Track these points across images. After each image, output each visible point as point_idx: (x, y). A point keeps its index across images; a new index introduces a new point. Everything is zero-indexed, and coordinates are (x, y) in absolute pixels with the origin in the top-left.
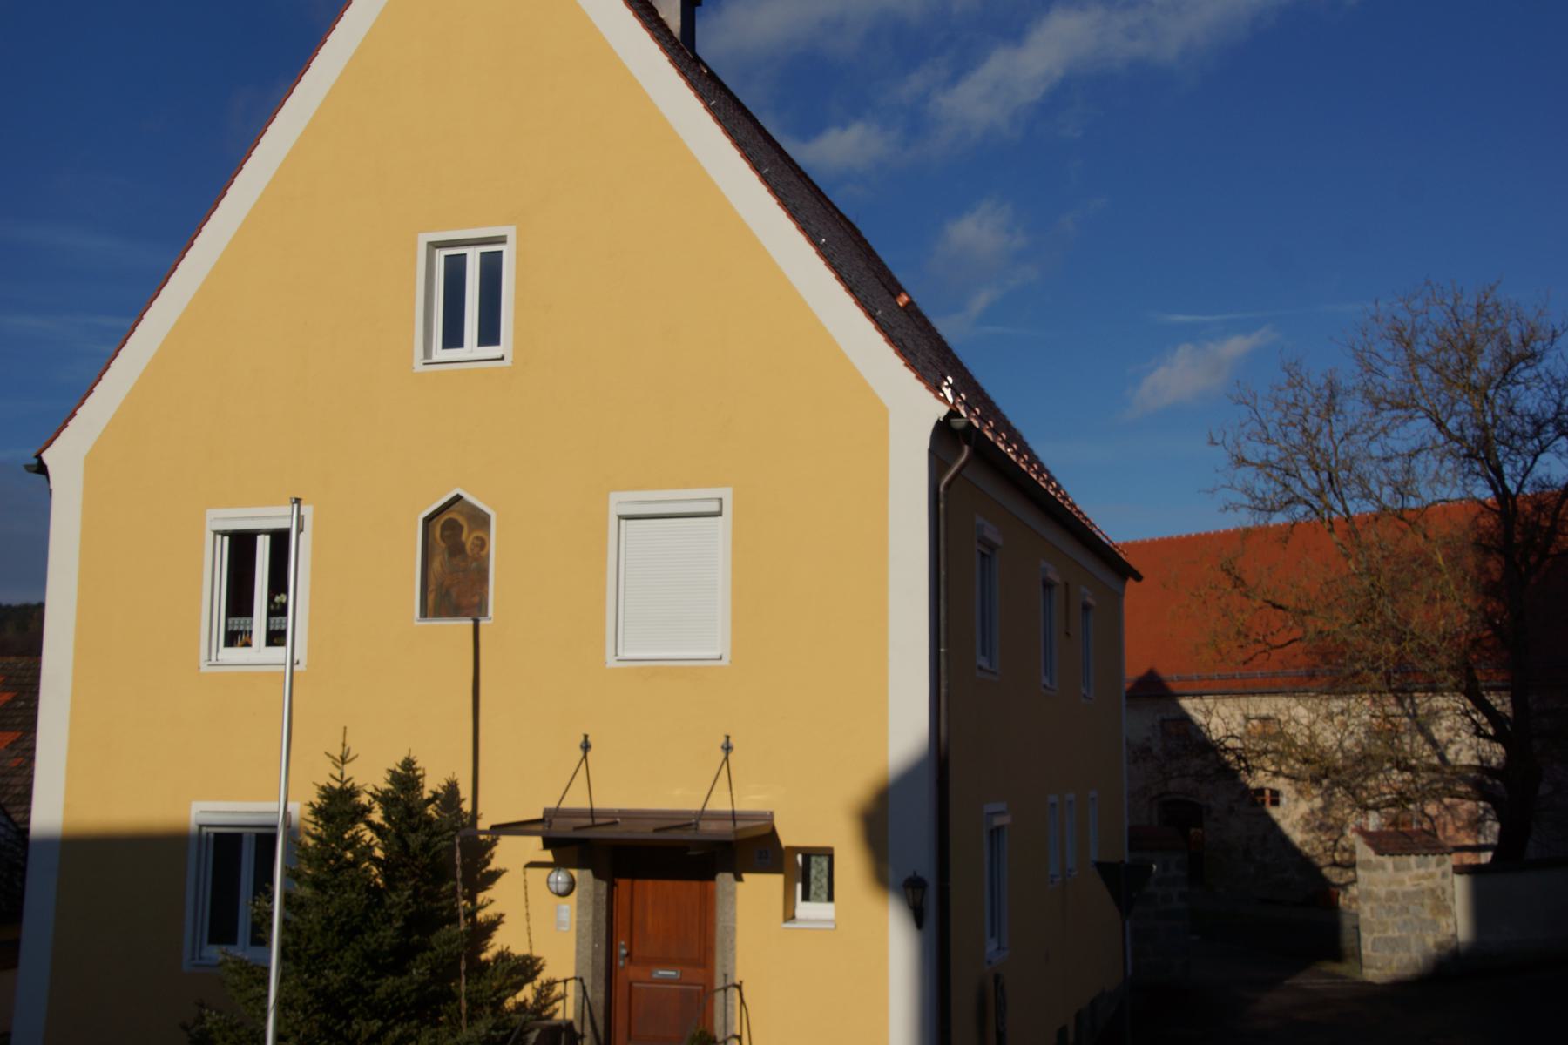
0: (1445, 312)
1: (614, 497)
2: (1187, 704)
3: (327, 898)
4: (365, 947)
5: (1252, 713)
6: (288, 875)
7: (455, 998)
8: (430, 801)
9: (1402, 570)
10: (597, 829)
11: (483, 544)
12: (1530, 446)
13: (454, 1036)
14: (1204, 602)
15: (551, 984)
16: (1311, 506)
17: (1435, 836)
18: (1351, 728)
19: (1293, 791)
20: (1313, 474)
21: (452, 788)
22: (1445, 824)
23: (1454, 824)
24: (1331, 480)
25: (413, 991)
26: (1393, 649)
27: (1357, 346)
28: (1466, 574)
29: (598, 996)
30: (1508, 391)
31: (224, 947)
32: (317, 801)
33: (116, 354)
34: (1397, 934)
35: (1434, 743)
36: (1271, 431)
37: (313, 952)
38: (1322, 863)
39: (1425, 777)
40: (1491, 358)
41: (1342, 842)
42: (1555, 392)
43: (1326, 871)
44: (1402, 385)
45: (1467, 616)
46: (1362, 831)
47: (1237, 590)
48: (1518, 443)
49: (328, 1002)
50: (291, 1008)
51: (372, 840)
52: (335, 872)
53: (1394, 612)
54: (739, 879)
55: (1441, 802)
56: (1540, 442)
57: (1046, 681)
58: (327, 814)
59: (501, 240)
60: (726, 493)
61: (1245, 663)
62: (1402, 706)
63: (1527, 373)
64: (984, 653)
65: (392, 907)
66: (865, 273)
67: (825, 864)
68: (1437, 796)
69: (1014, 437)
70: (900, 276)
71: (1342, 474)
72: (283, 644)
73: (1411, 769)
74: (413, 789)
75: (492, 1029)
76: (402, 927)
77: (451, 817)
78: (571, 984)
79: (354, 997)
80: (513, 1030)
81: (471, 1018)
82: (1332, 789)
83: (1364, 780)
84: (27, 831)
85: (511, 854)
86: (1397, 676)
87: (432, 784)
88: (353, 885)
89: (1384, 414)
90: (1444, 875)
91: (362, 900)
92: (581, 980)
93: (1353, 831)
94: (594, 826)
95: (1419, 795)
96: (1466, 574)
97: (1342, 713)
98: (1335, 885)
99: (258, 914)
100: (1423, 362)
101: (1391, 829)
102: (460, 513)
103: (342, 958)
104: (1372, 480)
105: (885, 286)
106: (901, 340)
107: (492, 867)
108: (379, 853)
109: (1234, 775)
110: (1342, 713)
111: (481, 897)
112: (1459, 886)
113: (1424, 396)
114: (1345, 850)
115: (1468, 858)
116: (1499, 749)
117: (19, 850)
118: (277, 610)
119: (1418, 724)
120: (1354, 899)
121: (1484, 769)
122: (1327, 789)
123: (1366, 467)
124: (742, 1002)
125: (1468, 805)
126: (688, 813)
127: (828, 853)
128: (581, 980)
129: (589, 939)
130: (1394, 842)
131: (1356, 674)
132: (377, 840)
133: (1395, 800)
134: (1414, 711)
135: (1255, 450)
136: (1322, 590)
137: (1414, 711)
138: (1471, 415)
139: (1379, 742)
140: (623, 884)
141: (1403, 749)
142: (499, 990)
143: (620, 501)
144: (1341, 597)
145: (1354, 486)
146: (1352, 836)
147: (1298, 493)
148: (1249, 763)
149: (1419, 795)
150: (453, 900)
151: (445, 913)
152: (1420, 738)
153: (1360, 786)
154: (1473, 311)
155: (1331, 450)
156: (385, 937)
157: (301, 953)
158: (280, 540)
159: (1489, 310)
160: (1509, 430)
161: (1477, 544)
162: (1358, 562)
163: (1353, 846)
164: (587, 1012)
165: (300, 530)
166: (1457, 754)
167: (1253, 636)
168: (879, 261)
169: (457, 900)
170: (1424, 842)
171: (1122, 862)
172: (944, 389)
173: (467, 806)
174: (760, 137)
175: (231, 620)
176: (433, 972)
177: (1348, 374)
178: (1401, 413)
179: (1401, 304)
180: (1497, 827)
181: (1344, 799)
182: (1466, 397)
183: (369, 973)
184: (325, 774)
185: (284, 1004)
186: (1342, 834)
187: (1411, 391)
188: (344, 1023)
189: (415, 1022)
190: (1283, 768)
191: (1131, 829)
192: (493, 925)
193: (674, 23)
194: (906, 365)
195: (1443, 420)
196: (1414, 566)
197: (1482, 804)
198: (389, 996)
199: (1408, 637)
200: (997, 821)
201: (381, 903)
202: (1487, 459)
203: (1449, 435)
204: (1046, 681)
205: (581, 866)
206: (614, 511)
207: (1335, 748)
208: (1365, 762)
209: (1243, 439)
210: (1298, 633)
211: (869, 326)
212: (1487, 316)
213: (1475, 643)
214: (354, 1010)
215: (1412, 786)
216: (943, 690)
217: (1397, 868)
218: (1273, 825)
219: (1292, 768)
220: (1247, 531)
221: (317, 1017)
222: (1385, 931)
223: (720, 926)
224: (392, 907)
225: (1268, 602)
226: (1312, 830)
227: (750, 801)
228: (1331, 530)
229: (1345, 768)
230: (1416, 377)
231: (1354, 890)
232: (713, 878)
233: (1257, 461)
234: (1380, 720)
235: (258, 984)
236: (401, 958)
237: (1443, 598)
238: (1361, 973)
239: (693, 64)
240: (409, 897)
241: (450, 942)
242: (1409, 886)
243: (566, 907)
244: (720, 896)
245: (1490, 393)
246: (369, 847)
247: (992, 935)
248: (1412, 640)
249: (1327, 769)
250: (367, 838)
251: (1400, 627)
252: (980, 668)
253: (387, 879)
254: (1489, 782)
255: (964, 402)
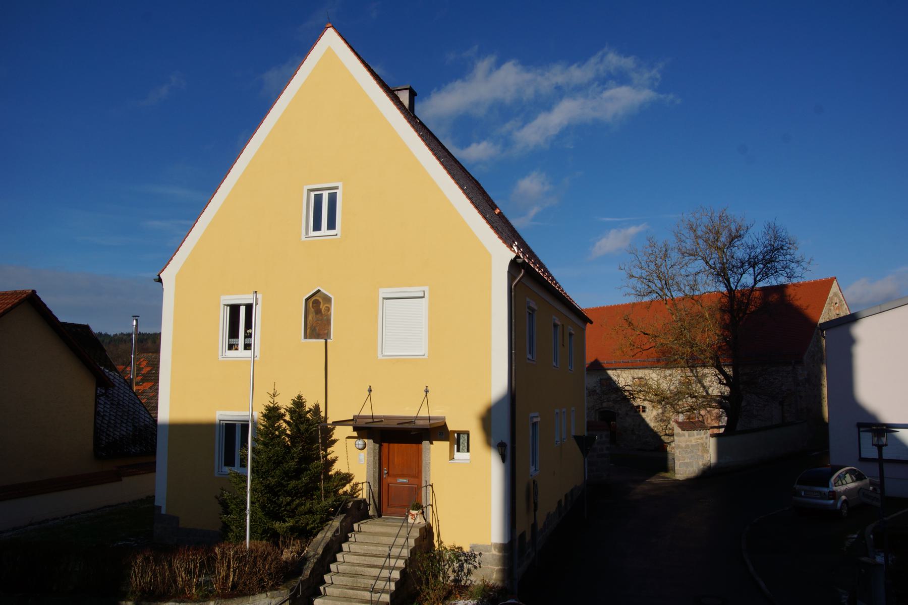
0: (708, 218)
1: (382, 290)
2: (610, 372)
3: (269, 450)
4: (284, 469)
5: (636, 376)
6: (253, 440)
7: (319, 489)
8: (308, 412)
9: (693, 319)
10: (374, 423)
11: (329, 309)
12: (739, 271)
13: (319, 504)
14: (617, 332)
15: (357, 484)
16: (658, 294)
17: (704, 423)
18: (673, 382)
19: (651, 406)
20: (659, 281)
21: (317, 407)
22: (707, 418)
23: (711, 418)
24: (666, 284)
25: (303, 486)
26: (689, 350)
27: (675, 231)
28: (717, 321)
29: (376, 489)
30: (731, 250)
31: (230, 468)
32: (264, 412)
33: (188, 235)
34: (689, 461)
35: (704, 387)
36: (643, 264)
37: (264, 470)
38: (661, 435)
39: (701, 400)
40: (725, 237)
41: (669, 426)
42: (748, 250)
43: (662, 437)
44: (692, 247)
45: (717, 337)
46: (677, 422)
47: (630, 327)
48: (735, 270)
49: (270, 489)
50: (256, 492)
51: (285, 427)
52: (272, 439)
53: (690, 336)
54: (432, 443)
55: (706, 410)
56: (743, 270)
57: (555, 364)
58: (268, 416)
59: (337, 188)
60: (426, 289)
61: (633, 356)
62: (693, 373)
63: (738, 243)
64: (530, 353)
65: (294, 453)
66: (482, 200)
67: (466, 437)
68: (705, 407)
69: (542, 266)
70: (496, 202)
71: (670, 281)
72: (250, 349)
73: (695, 397)
74: (302, 406)
75: (334, 501)
76: (298, 461)
77: (316, 418)
78: (365, 484)
79: (280, 488)
80: (343, 502)
81: (326, 497)
82: (666, 405)
83: (678, 402)
84: (157, 420)
85: (341, 433)
86: (691, 361)
87: (309, 405)
88: (279, 444)
89: (686, 258)
90: (707, 438)
91: (282, 451)
92: (369, 483)
93: (673, 421)
94: (373, 422)
95: (698, 407)
96: (717, 321)
97: (670, 376)
98: (666, 443)
99: (242, 455)
100: (700, 238)
101: (688, 421)
102: (320, 297)
103: (275, 473)
104: (682, 284)
105: (490, 205)
106: (497, 227)
107: (333, 438)
108: (288, 432)
109: (628, 400)
110: (670, 376)
111: (329, 450)
112: (712, 442)
113: (701, 251)
114: (670, 429)
115: (716, 431)
116: (728, 389)
117: (154, 427)
118: (248, 336)
119: (698, 379)
120: (673, 448)
121: (722, 396)
122: (664, 406)
123: (679, 279)
124: (433, 491)
125: (716, 410)
126: (411, 417)
127: (467, 433)
128: (369, 483)
129: (372, 467)
130: (689, 425)
131: (675, 360)
132: (288, 427)
133: (689, 409)
134: (697, 374)
135: (637, 272)
136: (663, 327)
137: (697, 374)
138: (718, 259)
139: (684, 387)
140: (385, 445)
141: (692, 390)
142: (337, 486)
143: (384, 292)
144: (670, 330)
145: (674, 286)
146: (673, 424)
147: (654, 289)
148: (634, 396)
149: (698, 407)
150: (318, 451)
151: (315, 456)
152: (699, 385)
153: (676, 404)
154: (718, 219)
155: (666, 272)
156: (292, 465)
157: (259, 471)
158: (249, 308)
159: (724, 218)
160: (732, 265)
161: (721, 309)
162: (676, 316)
163: (673, 427)
164: (371, 495)
165: (257, 304)
166: (712, 391)
167: (636, 346)
168: (487, 196)
169: (319, 451)
170: (699, 425)
171: (584, 435)
172: (514, 247)
173: (323, 414)
174: (440, 147)
175: (230, 340)
176: (310, 479)
177: (672, 242)
178: (692, 257)
179: (691, 215)
180: (726, 418)
181: (670, 409)
182: (716, 252)
183: (286, 479)
184: (267, 401)
185: (253, 490)
186: (669, 423)
187: (696, 249)
188: (276, 498)
189: (304, 498)
190: (647, 398)
191: (587, 422)
192: (334, 461)
193: (406, 102)
194: (498, 237)
195: (708, 260)
196: (697, 318)
197: (721, 410)
198: (294, 488)
199: (695, 346)
200: (535, 420)
201: (290, 452)
202: (724, 276)
203: (710, 266)
204: (555, 364)
205: (368, 438)
206: (381, 296)
207: (667, 389)
208: (678, 395)
209: (632, 267)
210: (653, 344)
211: (484, 221)
212: (723, 220)
213: (720, 347)
214: (280, 493)
215: (696, 404)
216: (513, 368)
217: (689, 436)
218: (643, 420)
219: (650, 397)
220: (634, 304)
221: (266, 495)
222: (684, 460)
223: (424, 462)
224: (294, 453)
225: (642, 332)
226: (658, 422)
227: (436, 412)
228: (666, 304)
229: (671, 397)
230: (698, 244)
231: (673, 445)
232: (421, 443)
233: (637, 276)
234: (684, 378)
235: (243, 482)
236: (297, 474)
237: (708, 330)
238: (675, 476)
239: (413, 119)
240: (301, 449)
241: (317, 467)
242: (693, 442)
243: (362, 454)
244: (424, 450)
245: (725, 250)
246: (285, 430)
247: (533, 465)
248: (696, 347)
249: (664, 397)
250: (284, 426)
251: (692, 342)
252: (528, 359)
253: (292, 442)
254: (724, 402)
255: (522, 252)
